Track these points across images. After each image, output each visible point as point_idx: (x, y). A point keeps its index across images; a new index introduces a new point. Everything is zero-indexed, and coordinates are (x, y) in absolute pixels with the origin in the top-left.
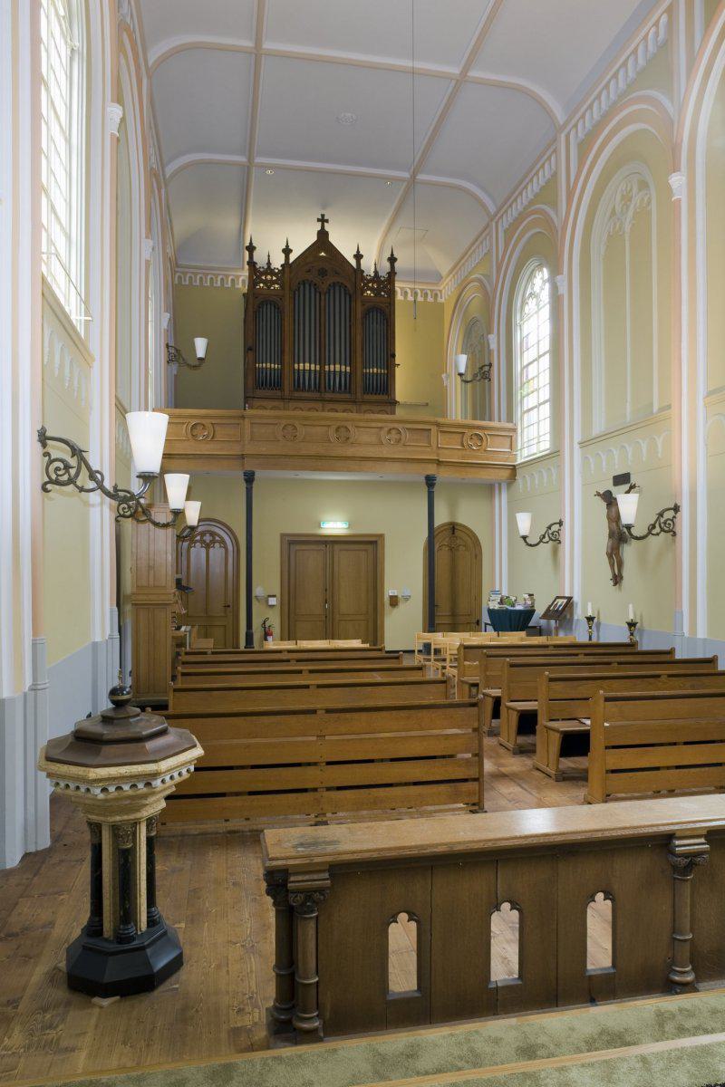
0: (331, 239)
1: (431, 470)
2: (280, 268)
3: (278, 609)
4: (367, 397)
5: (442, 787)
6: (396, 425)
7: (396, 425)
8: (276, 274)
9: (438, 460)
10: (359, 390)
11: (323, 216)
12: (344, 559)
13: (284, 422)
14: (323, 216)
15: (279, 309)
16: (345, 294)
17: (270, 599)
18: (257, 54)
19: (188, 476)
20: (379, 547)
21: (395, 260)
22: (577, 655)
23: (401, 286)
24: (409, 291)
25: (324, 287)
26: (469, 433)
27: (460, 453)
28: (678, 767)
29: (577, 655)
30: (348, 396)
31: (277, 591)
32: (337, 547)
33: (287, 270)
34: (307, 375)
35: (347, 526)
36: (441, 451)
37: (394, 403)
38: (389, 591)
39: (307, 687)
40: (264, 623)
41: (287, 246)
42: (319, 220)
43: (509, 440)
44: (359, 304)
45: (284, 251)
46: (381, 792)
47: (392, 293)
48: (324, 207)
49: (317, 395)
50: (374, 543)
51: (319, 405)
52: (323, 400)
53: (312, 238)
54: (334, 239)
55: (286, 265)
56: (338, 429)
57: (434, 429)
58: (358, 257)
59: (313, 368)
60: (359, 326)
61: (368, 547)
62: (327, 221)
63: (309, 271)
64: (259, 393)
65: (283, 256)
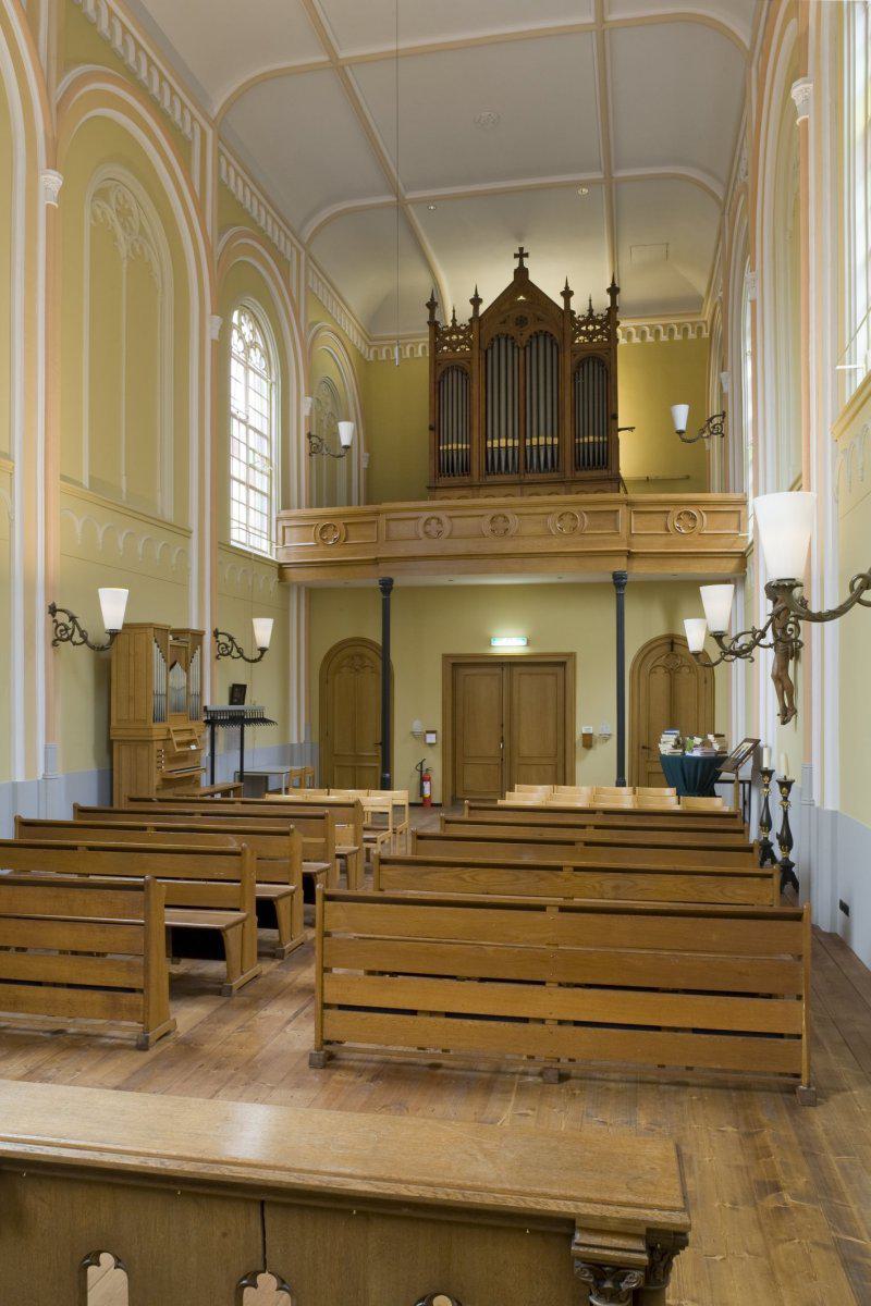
0: (532, 278)
1: (620, 565)
2: (468, 324)
3: (439, 749)
4: (581, 474)
5: (97, 996)
6: (502, 511)
7: (502, 511)
8: (462, 333)
9: (629, 552)
10: (568, 467)
11: (521, 249)
12: (528, 690)
13: (427, 515)
14: (521, 249)
15: (466, 375)
16: (513, 347)
17: (428, 735)
18: (338, 68)
19: (100, 590)
20: (569, 671)
21: (571, 293)
22: (584, 827)
23: (663, 322)
24: (633, 330)
25: (523, 340)
26: (675, 511)
27: (664, 539)
28: (449, 1015)
29: (584, 827)
30: (555, 475)
31: (437, 724)
32: (517, 670)
33: (475, 326)
34: (510, 452)
35: (524, 643)
36: (634, 540)
37: (616, 481)
38: (582, 727)
39: (74, 848)
40: (421, 764)
41: (476, 295)
42: (516, 256)
43: (391, 522)
44: (568, 353)
45: (472, 301)
46: (24, 991)
47: (613, 339)
48: (520, 236)
49: (515, 478)
50: (563, 664)
51: (517, 489)
52: (521, 484)
53: (508, 279)
54: (534, 278)
55: (475, 319)
56: (493, 520)
57: (623, 510)
58: (567, 294)
59: (510, 444)
60: (568, 383)
61: (553, 669)
62: (527, 255)
63: (504, 322)
64: (444, 481)
65: (471, 307)
